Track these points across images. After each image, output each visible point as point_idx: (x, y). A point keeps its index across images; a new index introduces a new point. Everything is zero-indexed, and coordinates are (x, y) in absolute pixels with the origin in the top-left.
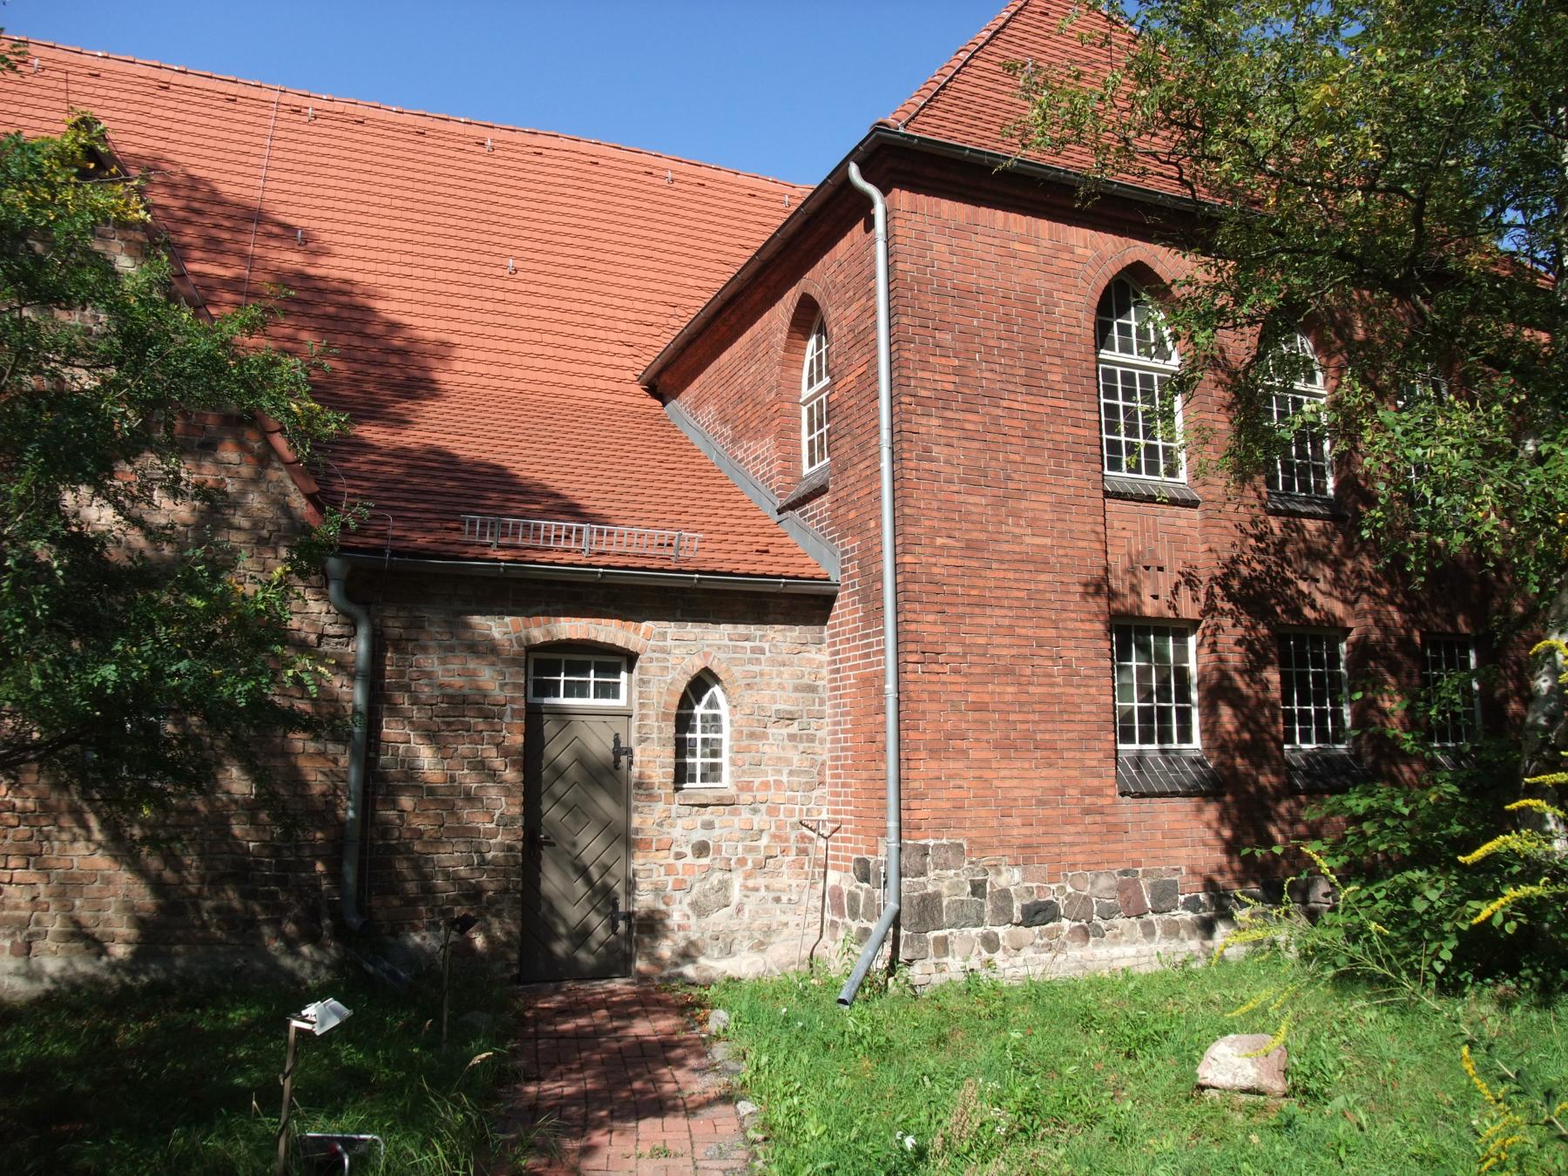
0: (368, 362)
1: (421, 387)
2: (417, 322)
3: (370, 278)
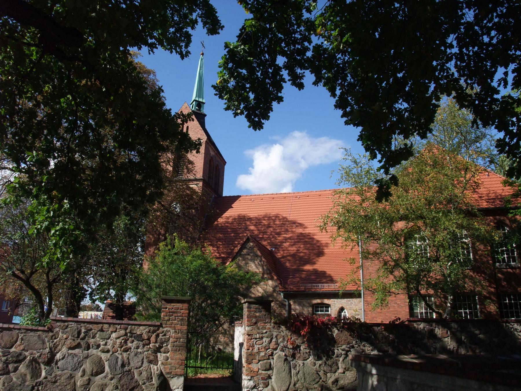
0: (37, 330)
1: (321, 254)
2: (322, 239)
3: (314, 232)
